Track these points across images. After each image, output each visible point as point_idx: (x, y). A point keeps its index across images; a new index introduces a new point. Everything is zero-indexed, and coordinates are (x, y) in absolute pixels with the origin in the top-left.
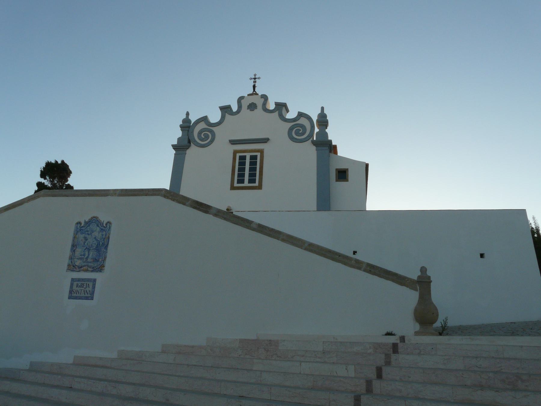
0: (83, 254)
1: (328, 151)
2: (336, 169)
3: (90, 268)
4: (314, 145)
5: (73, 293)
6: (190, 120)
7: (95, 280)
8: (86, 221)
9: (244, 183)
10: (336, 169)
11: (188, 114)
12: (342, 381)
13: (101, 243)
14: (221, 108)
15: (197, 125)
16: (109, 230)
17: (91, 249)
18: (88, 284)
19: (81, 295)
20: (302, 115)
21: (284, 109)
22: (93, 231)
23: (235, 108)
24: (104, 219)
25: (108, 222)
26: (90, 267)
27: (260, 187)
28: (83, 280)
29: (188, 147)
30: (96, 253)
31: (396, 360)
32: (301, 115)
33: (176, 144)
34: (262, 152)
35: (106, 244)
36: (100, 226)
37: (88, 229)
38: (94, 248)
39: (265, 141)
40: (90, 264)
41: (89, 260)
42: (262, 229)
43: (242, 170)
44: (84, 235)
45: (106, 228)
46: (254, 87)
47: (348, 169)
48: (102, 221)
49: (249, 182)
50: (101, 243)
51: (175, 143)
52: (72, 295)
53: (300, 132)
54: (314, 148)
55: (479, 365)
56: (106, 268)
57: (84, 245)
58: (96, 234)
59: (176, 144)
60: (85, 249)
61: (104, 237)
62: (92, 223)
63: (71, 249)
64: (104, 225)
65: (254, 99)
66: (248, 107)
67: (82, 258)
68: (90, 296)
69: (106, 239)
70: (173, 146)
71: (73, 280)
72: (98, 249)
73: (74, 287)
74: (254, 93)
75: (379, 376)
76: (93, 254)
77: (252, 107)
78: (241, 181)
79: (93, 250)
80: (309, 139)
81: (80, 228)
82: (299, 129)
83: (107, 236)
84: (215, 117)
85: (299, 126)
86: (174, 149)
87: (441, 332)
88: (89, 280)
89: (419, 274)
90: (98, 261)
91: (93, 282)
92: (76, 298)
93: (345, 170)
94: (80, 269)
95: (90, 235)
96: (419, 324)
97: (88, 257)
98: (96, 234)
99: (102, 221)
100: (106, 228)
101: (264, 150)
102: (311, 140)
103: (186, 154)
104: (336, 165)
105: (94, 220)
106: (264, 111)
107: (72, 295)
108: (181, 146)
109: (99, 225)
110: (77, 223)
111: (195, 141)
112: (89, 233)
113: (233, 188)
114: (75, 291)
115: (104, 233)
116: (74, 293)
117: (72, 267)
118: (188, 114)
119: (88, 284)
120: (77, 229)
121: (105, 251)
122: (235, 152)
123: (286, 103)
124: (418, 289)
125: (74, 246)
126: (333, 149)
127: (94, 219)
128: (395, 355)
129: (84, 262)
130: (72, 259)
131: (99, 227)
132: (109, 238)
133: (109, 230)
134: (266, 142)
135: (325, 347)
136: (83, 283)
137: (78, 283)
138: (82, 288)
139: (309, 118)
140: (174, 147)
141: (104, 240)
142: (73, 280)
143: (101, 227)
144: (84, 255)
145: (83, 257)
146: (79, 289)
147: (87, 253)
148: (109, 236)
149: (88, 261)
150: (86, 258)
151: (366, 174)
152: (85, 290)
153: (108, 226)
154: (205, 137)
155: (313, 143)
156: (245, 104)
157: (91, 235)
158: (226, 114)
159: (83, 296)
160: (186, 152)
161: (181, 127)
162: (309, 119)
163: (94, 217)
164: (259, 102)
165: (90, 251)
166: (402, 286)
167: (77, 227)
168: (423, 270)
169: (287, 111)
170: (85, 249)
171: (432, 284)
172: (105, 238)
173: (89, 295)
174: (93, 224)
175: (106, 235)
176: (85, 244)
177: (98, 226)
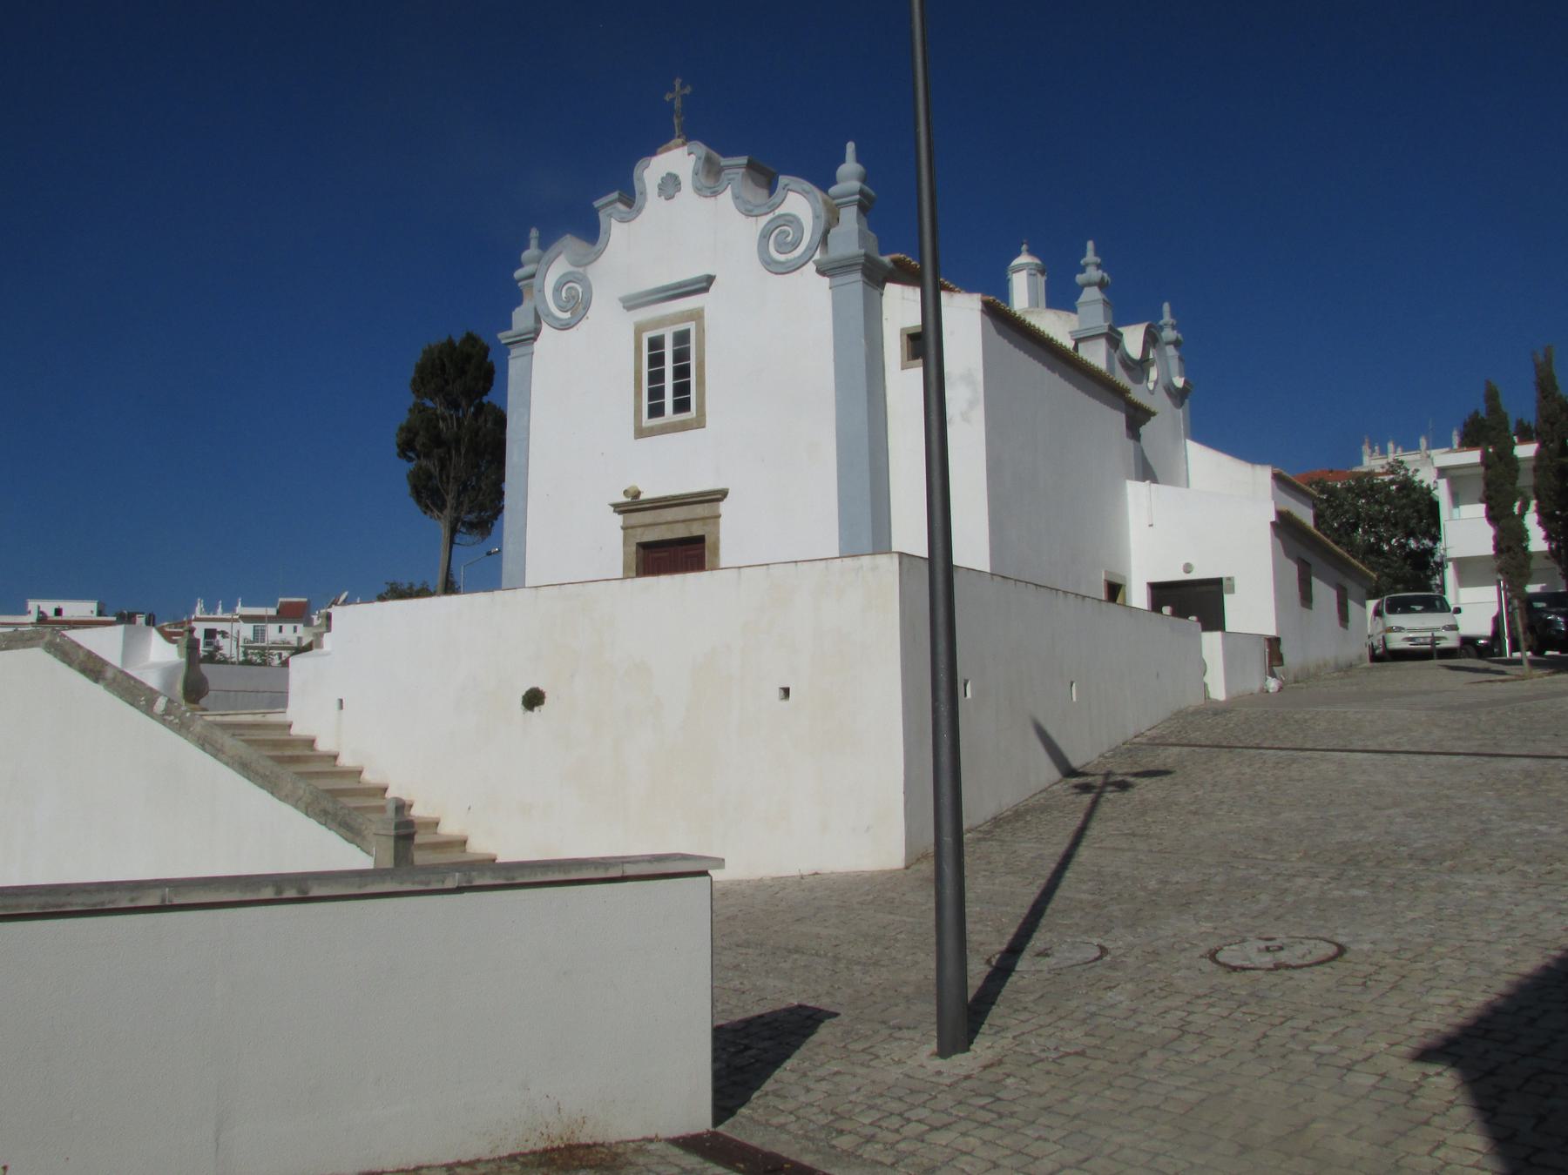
9: (206, 630)
15: (549, 266)
20: (787, 187)
27: (699, 423)
34: (697, 316)
85: (783, 223)
103: (533, 353)
111: (550, 314)
113: (641, 433)
122: (638, 332)
134: (706, 290)
154: (573, 310)
171: (722, 520)
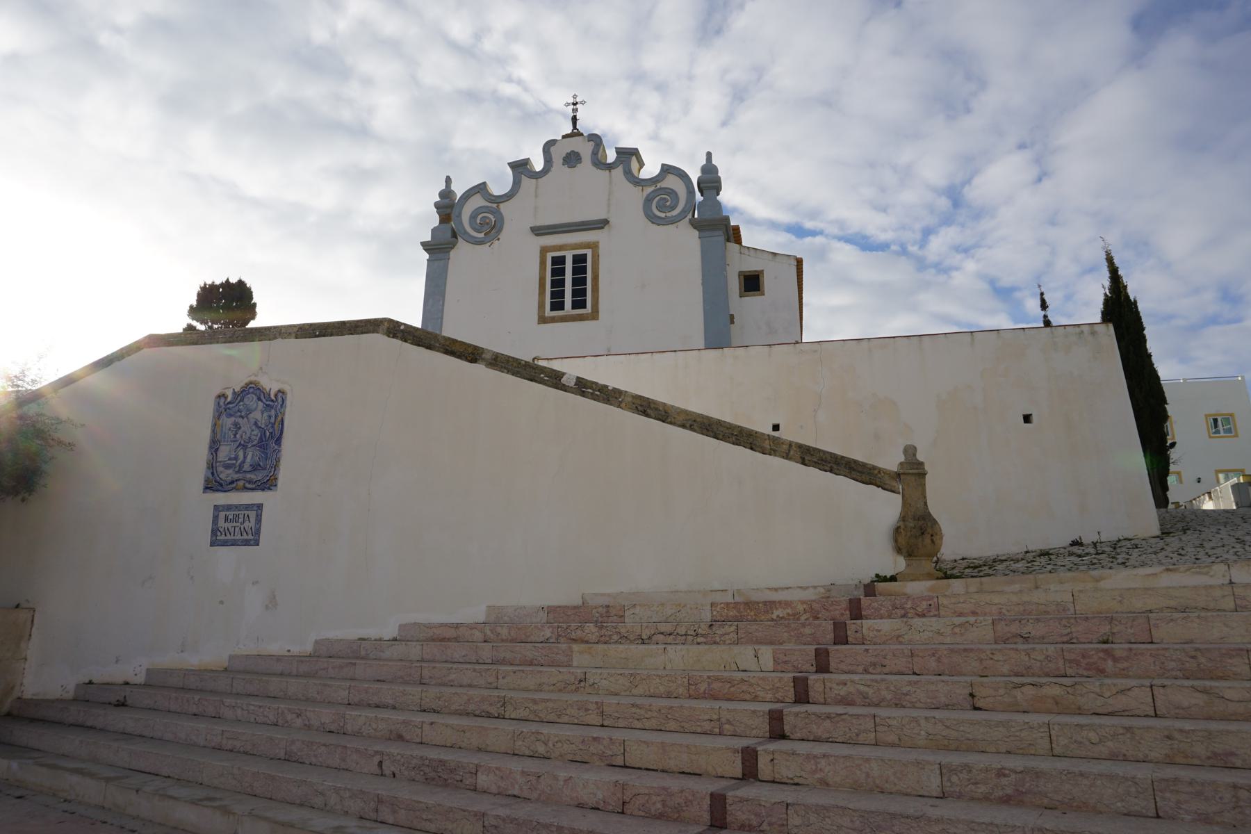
0: (233, 456)
1: (722, 239)
2: (740, 273)
3: (249, 484)
4: (695, 228)
5: (219, 534)
7: (260, 507)
8: (236, 390)
10: (740, 273)
11: (448, 180)
12: (746, 681)
13: (268, 434)
14: (514, 164)
16: (282, 406)
17: (250, 445)
18: (248, 516)
19: (236, 538)
21: (634, 158)
22: (250, 411)
23: (538, 165)
24: (270, 384)
25: (279, 391)
26: (250, 482)
27: (594, 315)
28: (238, 507)
29: (452, 246)
31: (856, 632)
32: (667, 170)
33: (430, 240)
34: (594, 246)
35: (277, 434)
36: (264, 400)
37: (241, 407)
38: (254, 443)
39: (602, 224)
40: (248, 476)
41: (247, 467)
43: (558, 283)
45: (275, 403)
47: (762, 271)
48: (268, 390)
49: (574, 307)
50: (268, 434)
51: (428, 238)
52: (218, 538)
53: (668, 204)
54: (696, 233)
55: (1027, 633)
57: (235, 439)
58: (257, 415)
59: (430, 240)
60: (237, 447)
61: (273, 420)
62: (247, 394)
63: (211, 448)
64: (273, 397)
67: (234, 464)
68: (252, 538)
69: (277, 424)
70: (423, 244)
71: (216, 508)
73: (219, 523)
74: (575, 133)
75: (822, 666)
76: (253, 455)
77: (572, 159)
80: (685, 218)
81: (226, 405)
82: (665, 199)
83: (279, 418)
84: (501, 184)
86: (425, 250)
87: (24, 660)
88: (248, 507)
89: (902, 459)
91: (257, 510)
92: (224, 544)
95: (246, 419)
96: (904, 557)
97: (244, 462)
98: (257, 415)
99: (268, 390)
100: (275, 403)
101: (598, 242)
102: (690, 219)
103: (449, 259)
104: (738, 264)
105: (252, 389)
107: (218, 538)
108: (444, 245)
109: (262, 398)
110: (219, 397)
111: (466, 232)
112: (243, 414)
113: (543, 320)
116: (221, 534)
117: (213, 484)
118: (448, 180)
119: (246, 515)
120: (220, 407)
121: (276, 447)
122: (544, 250)
123: (637, 149)
124: (901, 491)
125: (214, 446)
126: (734, 235)
127: (250, 386)
128: (854, 623)
129: (237, 472)
132: (282, 424)
133: (282, 406)
135: (714, 613)
136: (237, 513)
137: (228, 513)
138: (235, 524)
139: (683, 175)
140: (426, 246)
142: (216, 508)
143: (267, 401)
144: (236, 458)
145: (234, 462)
149: (244, 469)
150: (240, 465)
151: (798, 285)
152: (242, 529)
153: (280, 399)
155: (692, 225)
156: (558, 154)
157: (247, 418)
159: (238, 540)
160: (449, 255)
161: (437, 205)
162: (683, 177)
163: (251, 383)
164: (585, 149)
165: (247, 450)
167: (219, 403)
168: (910, 451)
169: (641, 164)
170: (237, 447)
172: (275, 424)
173: (250, 537)
174: (249, 396)
175: (276, 417)
177: (259, 399)
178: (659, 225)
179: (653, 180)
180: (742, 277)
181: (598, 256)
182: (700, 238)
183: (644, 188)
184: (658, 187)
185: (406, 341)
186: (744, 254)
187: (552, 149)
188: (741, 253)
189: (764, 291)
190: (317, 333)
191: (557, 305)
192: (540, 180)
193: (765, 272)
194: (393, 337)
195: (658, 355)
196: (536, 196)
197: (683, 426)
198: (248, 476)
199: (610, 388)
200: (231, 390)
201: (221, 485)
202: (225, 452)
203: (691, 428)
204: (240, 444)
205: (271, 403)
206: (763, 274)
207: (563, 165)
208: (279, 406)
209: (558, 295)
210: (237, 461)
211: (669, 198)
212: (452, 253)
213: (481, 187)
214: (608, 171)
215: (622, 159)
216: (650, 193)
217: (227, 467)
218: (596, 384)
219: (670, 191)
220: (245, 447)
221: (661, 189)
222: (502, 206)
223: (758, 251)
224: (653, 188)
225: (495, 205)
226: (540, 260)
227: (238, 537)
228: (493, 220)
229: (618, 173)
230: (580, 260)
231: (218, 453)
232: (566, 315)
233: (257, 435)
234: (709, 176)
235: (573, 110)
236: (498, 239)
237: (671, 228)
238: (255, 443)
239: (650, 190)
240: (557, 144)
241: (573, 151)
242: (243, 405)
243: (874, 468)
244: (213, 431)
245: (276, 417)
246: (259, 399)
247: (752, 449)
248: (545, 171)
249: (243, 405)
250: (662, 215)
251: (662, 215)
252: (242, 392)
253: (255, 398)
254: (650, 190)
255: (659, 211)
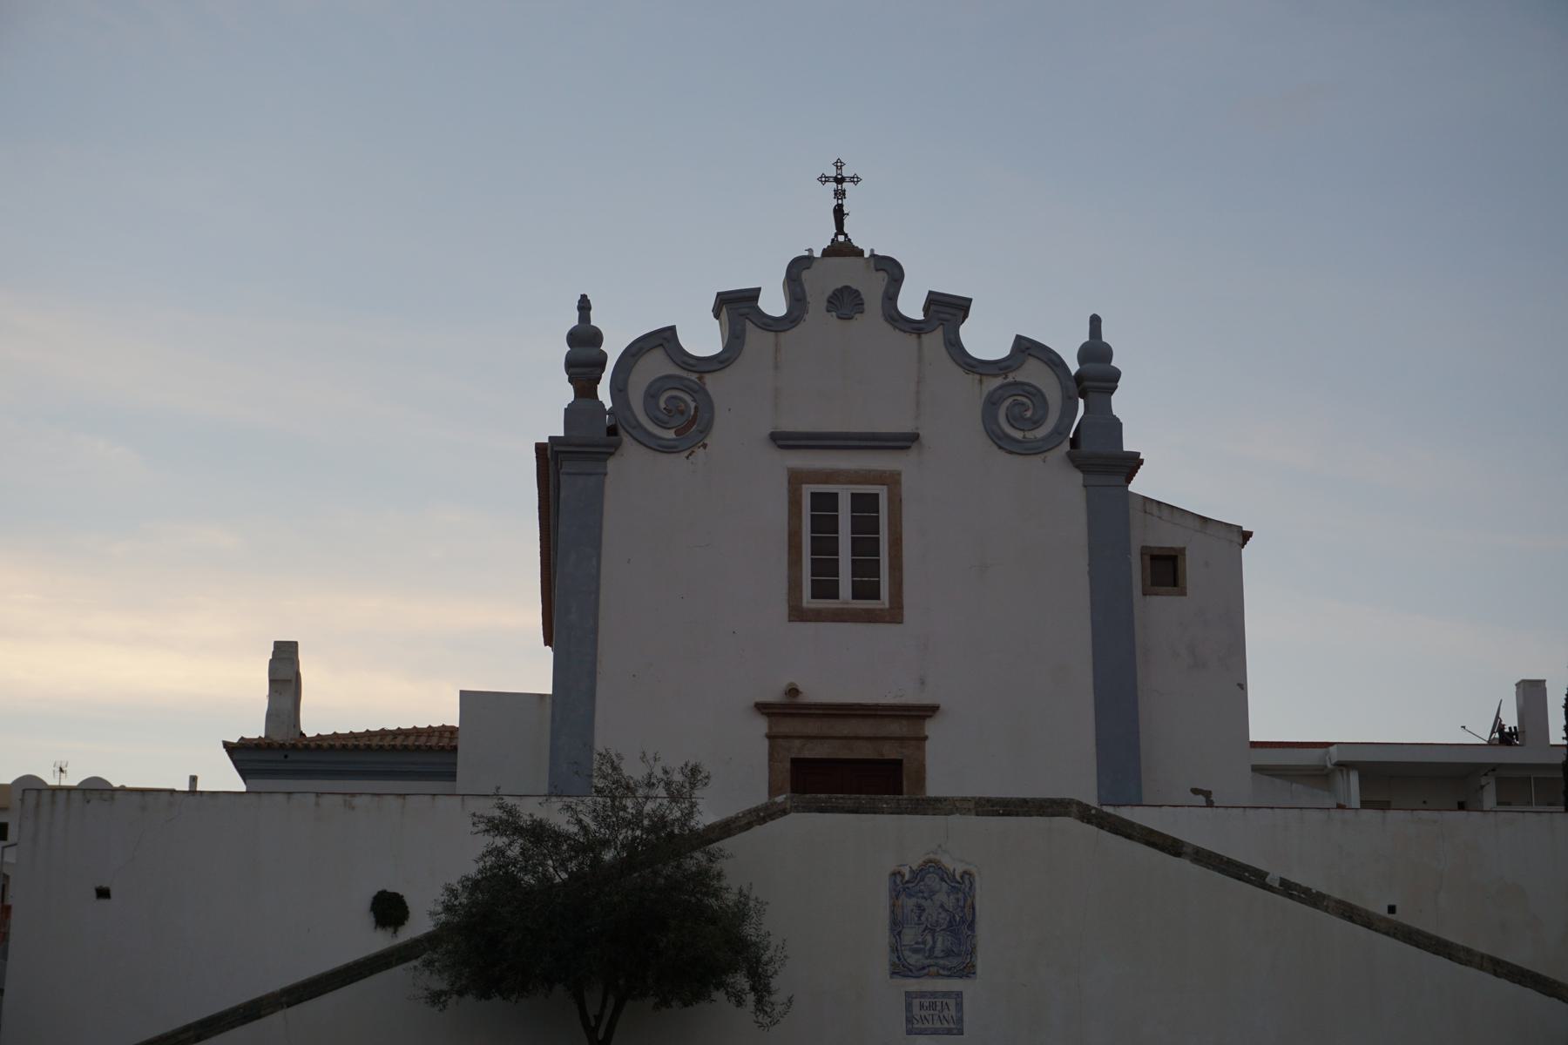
5: (915, 1022)
6: (597, 328)
7: (959, 995)
8: (915, 868)
13: (958, 919)
22: (933, 893)
23: (774, 303)
26: (944, 968)
27: (895, 615)
28: (933, 994)
30: (949, 938)
32: (1025, 348)
33: (562, 434)
34: (892, 480)
35: (969, 919)
37: (922, 887)
39: (904, 442)
40: (941, 962)
41: (938, 952)
42: (1288, 889)
44: (914, 900)
46: (839, 214)
53: (1028, 414)
56: (979, 970)
58: (941, 897)
60: (924, 931)
61: (961, 903)
63: (892, 930)
64: (958, 878)
65: (844, 273)
66: (829, 302)
67: (924, 949)
71: (908, 994)
72: (953, 928)
74: (841, 249)
77: (845, 302)
78: (824, 589)
79: (942, 932)
82: (1023, 404)
83: (969, 901)
88: (946, 994)
90: (456, 899)
91: (956, 999)
92: (921, 1032)
93: (1173, 553)
94: (920, 972)
97: (933, 948)
100: (962, 885)
103: (606, 474)
105: (932, 867)
106: (886, 320)
107: (916, 1026)
111: (639, 426)
112: (925, 895)
113: (798, 614)
114: (918, 1018)
115: (960, 896)
117: (900, 969)
119: (944, 1004)
121: (969, 933)
122: (796, 479)
125: (896, 926)
127: (930, 864)
129: (927, 958)
130: (897, 950)
131: (946, 882)
132: (974, 908)
133: (970, 888)
136: (934, 1000)
137: (923, 1000)
138: (932, 1012)
139: (1052, 360)
141: (962, 911)
142: (908, 994)
144: (924, 942)
145: (922, 946)
146: (923, 1013)
147: (929, 938)
148: (973, 903)
152: (942, 1017)
153: (967, 882)
156: (818, 287)
158: (748, 323)
160: (605, 467)
162: (1056, 365)
164: (871, 287)
166: (1514, 982)
167: (895, 882)
170: (924, 931)
172: (964, 907)
174: (930, 875)
175: (965, 900)
176: (922, 918)
178: (1011, 452)
179: (1004, 364)
180: (1147, 558)
181: (901, 500)
182: (1085, 486)
183: (984, 378)
184: (1010, 379)
185: (1102, 828)
186: (1151, 514)
187: (805, 275)
188: (1146, 512)
189: (1185, 588)
190: (1001, 812)
191: (824, 589)
192: (782, 335)
193: (1187, 552)
194: (1088, 823)
195: (1252, 811)
196: (776, 367)
197: (1387, 934)
198: (941, 962)
199: (1314, 891)
200: (907, 867)
201: (911, 971)
202: (909, 936)
203: (1395, 936)
204: (926, 928)
205: (957, 885)
206: (1184, 555)
207: (828, 311)
208: (967, 889)
209: (825, 569)
210: (925, 945)
211: (1031, 406)
212: (612, 464)
213: (668, 334)
214: (914, 336)
215: (942, 316)
216: (995, 390)
217: (916, 951)
218: (1300, 886)
219: (1032, 389)
220: (933, 932)
221: (1016, 384)
222: (708, 378)
223: (1175, 510)
224: (998, 382)
225: (694, 377)
226: (790, 498)
227: (938, 1025)
228: (693, 405)
229: (934, 340)
230: (865, 505)
231: (902, 936)
232: (843, 609)
233: (945, 919)
234: (1093, 367)
235: (836, 192)
236: (705, 446)
237: (1036, 460)
238: (944, 927)
239: (994, 383)
240: (815, 264)
241: (847, 288)
242: (925, 885)
243: (1555, 982)
244: (893, 912)
245: (965, 900)
246: (942, 879)
247: (1450, 959)
248: (792, 319)
249: (925, 885)
250: (1018, 435)
251: (1018, 435)
252: (920, 871)
253: (937, 880)
254: (994, 383)
255: (1014, 427)
